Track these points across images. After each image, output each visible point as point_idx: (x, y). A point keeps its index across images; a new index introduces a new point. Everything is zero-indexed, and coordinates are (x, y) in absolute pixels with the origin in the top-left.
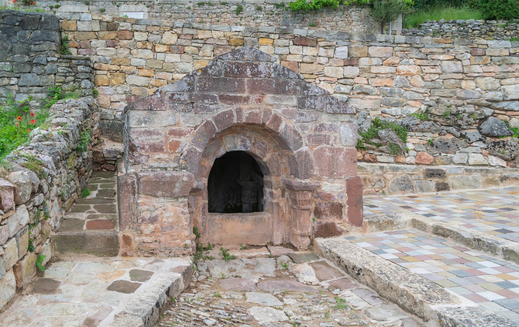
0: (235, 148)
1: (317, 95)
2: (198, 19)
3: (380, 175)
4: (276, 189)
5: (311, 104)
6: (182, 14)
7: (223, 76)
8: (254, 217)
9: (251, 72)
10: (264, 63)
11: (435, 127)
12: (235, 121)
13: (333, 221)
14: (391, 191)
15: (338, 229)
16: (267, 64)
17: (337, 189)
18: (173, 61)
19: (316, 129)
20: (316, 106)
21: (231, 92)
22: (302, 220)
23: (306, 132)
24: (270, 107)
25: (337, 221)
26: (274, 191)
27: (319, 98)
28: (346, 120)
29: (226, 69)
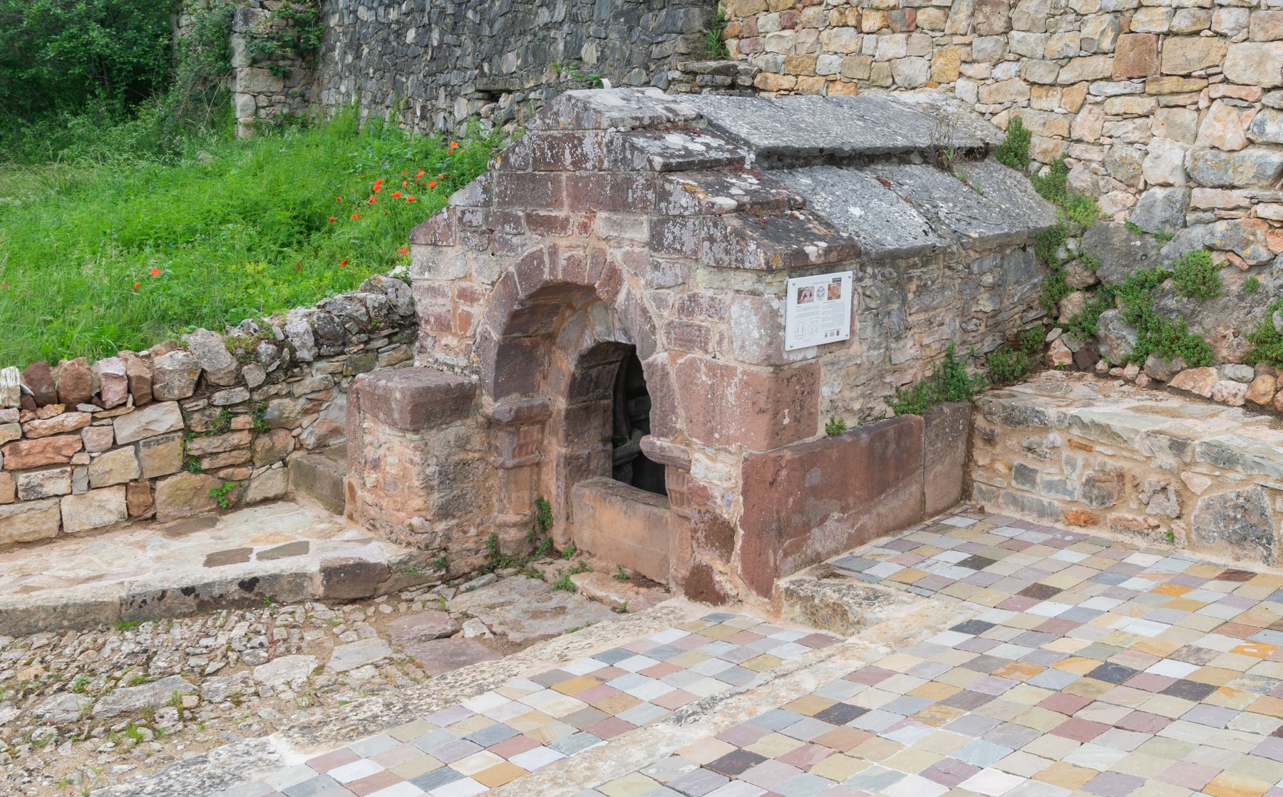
3: (1170, 471)
7: (530, 170)
10: (592, 133)
12: (546, 276)
13: (711, 563)
14: (1193, 536)
15: (717, 587)
17: (720, 480)
18: (890, 56)
19: (682, 309)
21: (541, 206)
23: (666, 313)
24: (603, 245)
25: (718, 565)
27: (690, 224)
28: (748, 286)
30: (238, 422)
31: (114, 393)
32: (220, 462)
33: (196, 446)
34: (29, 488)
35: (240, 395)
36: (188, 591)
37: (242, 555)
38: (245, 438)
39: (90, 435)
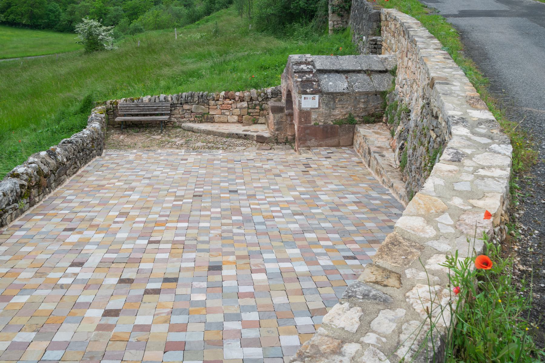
30: (257, 107)
31: (237, 98)
32: (254, 114)
33: (250, 111)
34: (223, 113)
35: (257, 102)
36: (237, 134)
37: (248, 131)
38: (258, 111)
39: (233, 105)
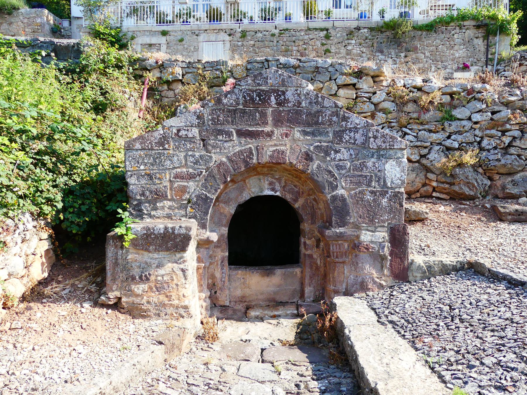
0: (261, 192)
1: (358, 127)
2: (283, 47)
4: (309, 239)
5: (350, 138)
6: (266, 43)
8: (283, 270)
9: (277, 100)
11: (518, 161)
16: (297, 90)
20: (356, 140)
22: (336, 274)
26: (308, 242)
27: (361, 131)
29: (245, 98)
